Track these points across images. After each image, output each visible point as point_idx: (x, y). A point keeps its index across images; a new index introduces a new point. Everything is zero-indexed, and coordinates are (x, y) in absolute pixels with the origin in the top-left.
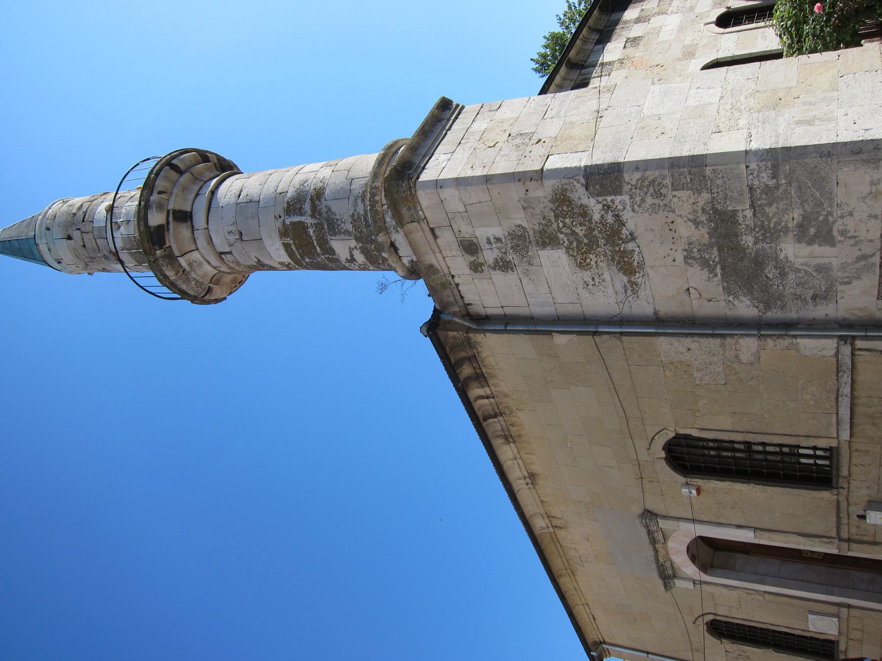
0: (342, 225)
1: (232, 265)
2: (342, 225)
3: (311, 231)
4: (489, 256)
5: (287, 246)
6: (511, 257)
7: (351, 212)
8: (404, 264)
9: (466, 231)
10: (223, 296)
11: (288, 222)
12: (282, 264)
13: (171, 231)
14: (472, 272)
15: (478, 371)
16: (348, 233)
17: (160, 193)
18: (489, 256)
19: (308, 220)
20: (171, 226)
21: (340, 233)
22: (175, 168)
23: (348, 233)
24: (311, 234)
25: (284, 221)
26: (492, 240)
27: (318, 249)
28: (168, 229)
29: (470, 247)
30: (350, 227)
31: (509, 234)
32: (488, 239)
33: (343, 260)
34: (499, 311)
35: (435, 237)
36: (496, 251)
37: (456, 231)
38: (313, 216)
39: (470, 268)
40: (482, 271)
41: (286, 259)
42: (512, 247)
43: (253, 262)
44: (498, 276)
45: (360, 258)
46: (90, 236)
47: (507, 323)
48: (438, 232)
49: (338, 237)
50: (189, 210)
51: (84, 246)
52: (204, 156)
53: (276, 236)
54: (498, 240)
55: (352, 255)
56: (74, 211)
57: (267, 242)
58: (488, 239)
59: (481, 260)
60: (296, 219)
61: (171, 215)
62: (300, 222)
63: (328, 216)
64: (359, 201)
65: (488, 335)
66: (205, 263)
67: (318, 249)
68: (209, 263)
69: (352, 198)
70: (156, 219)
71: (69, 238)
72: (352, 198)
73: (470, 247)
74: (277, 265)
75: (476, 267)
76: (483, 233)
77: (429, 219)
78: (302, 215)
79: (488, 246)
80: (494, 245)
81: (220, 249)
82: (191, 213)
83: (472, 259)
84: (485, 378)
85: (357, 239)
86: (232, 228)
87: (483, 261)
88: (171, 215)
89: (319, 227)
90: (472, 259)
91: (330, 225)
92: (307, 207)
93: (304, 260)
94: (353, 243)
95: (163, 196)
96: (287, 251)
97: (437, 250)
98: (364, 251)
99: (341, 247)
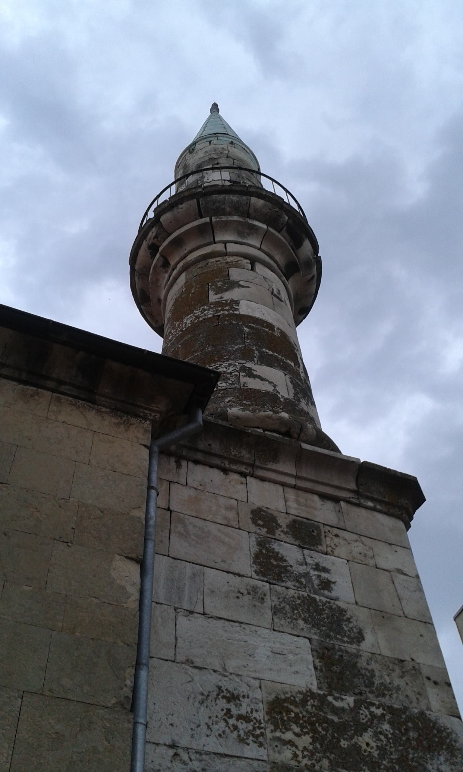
59: (278, 534)
66: (240, 240)
68: (236, 242)
95: (309, 277)
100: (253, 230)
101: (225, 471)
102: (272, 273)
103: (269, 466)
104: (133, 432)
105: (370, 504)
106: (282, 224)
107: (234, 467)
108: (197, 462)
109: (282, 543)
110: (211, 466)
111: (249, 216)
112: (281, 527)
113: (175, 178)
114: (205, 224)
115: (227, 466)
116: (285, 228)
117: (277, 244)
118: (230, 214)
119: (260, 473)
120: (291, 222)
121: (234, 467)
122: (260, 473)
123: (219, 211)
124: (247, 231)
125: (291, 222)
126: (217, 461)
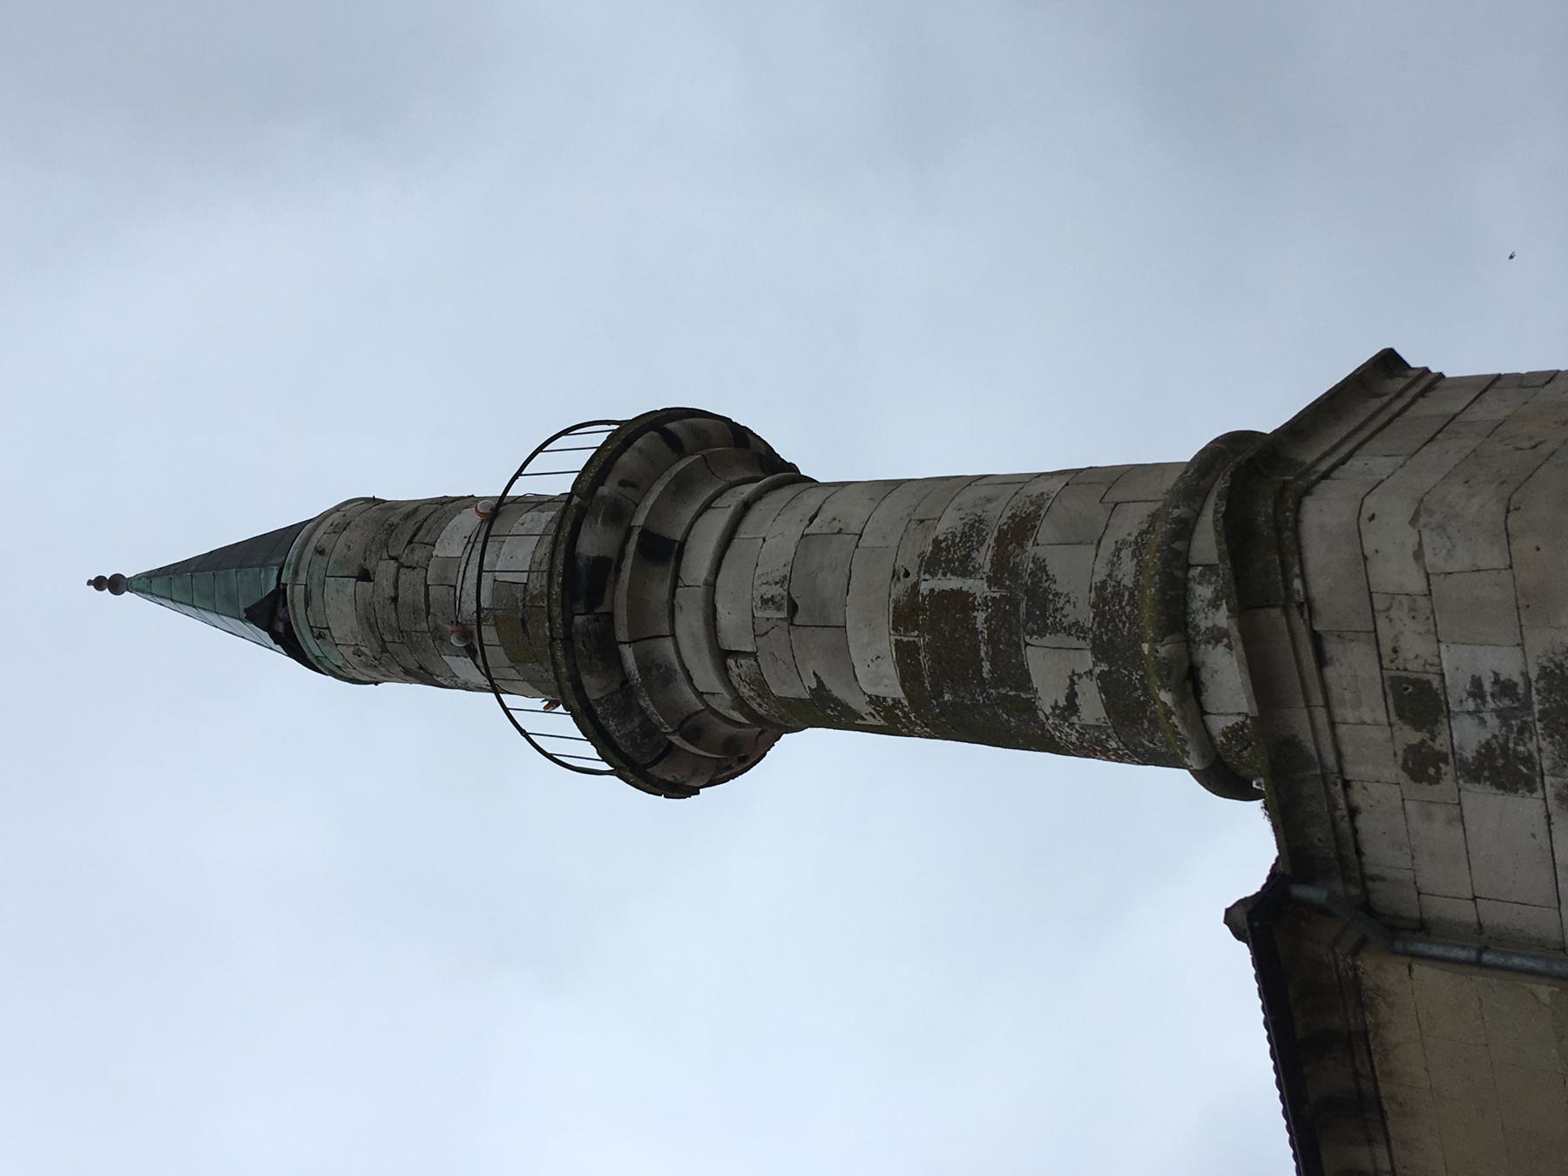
0: (1069, 608)
1: (746, 691)
2: (1069, 608)
3: (981, 616)
4: (1467, 734)
5: (905, 653)
6: (1532, 747)
7: (1097, 579)
8: (1211, 738)
9: (1415, 649)
10: (693, 783)
11: (924, 588)
12: (875, 701)
13: (625, 575)
14: (1404, 777)
15: (1366, 1086)
16: (1077, 630)
17: (623, 483)
18: (1467, 734)
19: (977, 587)
20: (628, 563)
21: (1056, 629)
22: (672, 440)
23: (1077, 630)
24: (980, 625)
25: (916, 585)
26: (1488, 687)
27: (986, 666)
28: (618, 570)
29: (1418, 701)
30: (1086, 616)
31: (1545, 673)
32: (1477, 682)
33: (1045, 705)
34: (1466, 912)
35: (1321, 660)
36: (1493, 722)
37: (1386, 649)
38: (993, 581)
39: (1404, 767)
40: (1436, 780)
41: (892, 689)
42: (1544, 715)
43: (798, 690)
44: (1484, 803)
45: (1092, 708)
46: (417, 576)
47: (1486, 949)
48: (1332, 648)
49: (1048, 640)
50: (678, 537)
51: (395, 599)
52: (741, 437)
53: (884, 621)
54: (1505, 688)
55: (1072, 696)
56: (394, 519)
57: (858, 639)
58: (1477, 682)
59: (1441, 744)
60: (953, 583)
61: (634, 538)
62: (958, 593)
63: (1037, 584)
64: (1126, 554)
65: (1423, 971)
66: (681, 675)
67: (986, 666)
68: (690, 679)
69: (1108, 545)
70: (593, 541)
71: (365, 576)
72: (1108, 545)
73: (1418, 701)
74: (860, 705)
75: (1421, 765)
76: (1469, 661)
77: (1318, 605)
78: (964, 573)
79: (1470, 705)
80: (1491, 704)
81: (729, 641)
82: (683, 544)
83: (1414, 737)
84: (1382, 1112)
85: (1101, 651)
86: (776, 591)
87: (1446, 749)
88: (634, 538)
89: (1003, 612)
90: (1414, 737)
91: (1029, 604)
92: (984, 557)
93: (941, 695)
94: (1086, 661)
95: (628, 491)
96: (900, 662)
97: (1318, 699)
98: (1109, 685)
99: (1052, 668)
100: (645, 665)
101: (1353, 812)
102: (719, 608)
103: (1313, 752)
104: (1027, 644)
105: (1297, 584)
106: (597, 620)
107: (1342, 803)
108: (1359, 853)
109: (1456, 744)
110: (1355, 831)
111: (626, 681)
112: (1423, 741)
113: (480, 689)
114: (685, 737)
115: (1345, 813)
116: (599, 610)
117: (637, 606)
118: (642, 711)
119: (1330, 759)
120: (580, 607)
121: (1342, 803)
122: (1330, 759)
123: (649, 730)
124: (654, 672)
125: (580, 607)
126: (1345, 825)
